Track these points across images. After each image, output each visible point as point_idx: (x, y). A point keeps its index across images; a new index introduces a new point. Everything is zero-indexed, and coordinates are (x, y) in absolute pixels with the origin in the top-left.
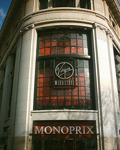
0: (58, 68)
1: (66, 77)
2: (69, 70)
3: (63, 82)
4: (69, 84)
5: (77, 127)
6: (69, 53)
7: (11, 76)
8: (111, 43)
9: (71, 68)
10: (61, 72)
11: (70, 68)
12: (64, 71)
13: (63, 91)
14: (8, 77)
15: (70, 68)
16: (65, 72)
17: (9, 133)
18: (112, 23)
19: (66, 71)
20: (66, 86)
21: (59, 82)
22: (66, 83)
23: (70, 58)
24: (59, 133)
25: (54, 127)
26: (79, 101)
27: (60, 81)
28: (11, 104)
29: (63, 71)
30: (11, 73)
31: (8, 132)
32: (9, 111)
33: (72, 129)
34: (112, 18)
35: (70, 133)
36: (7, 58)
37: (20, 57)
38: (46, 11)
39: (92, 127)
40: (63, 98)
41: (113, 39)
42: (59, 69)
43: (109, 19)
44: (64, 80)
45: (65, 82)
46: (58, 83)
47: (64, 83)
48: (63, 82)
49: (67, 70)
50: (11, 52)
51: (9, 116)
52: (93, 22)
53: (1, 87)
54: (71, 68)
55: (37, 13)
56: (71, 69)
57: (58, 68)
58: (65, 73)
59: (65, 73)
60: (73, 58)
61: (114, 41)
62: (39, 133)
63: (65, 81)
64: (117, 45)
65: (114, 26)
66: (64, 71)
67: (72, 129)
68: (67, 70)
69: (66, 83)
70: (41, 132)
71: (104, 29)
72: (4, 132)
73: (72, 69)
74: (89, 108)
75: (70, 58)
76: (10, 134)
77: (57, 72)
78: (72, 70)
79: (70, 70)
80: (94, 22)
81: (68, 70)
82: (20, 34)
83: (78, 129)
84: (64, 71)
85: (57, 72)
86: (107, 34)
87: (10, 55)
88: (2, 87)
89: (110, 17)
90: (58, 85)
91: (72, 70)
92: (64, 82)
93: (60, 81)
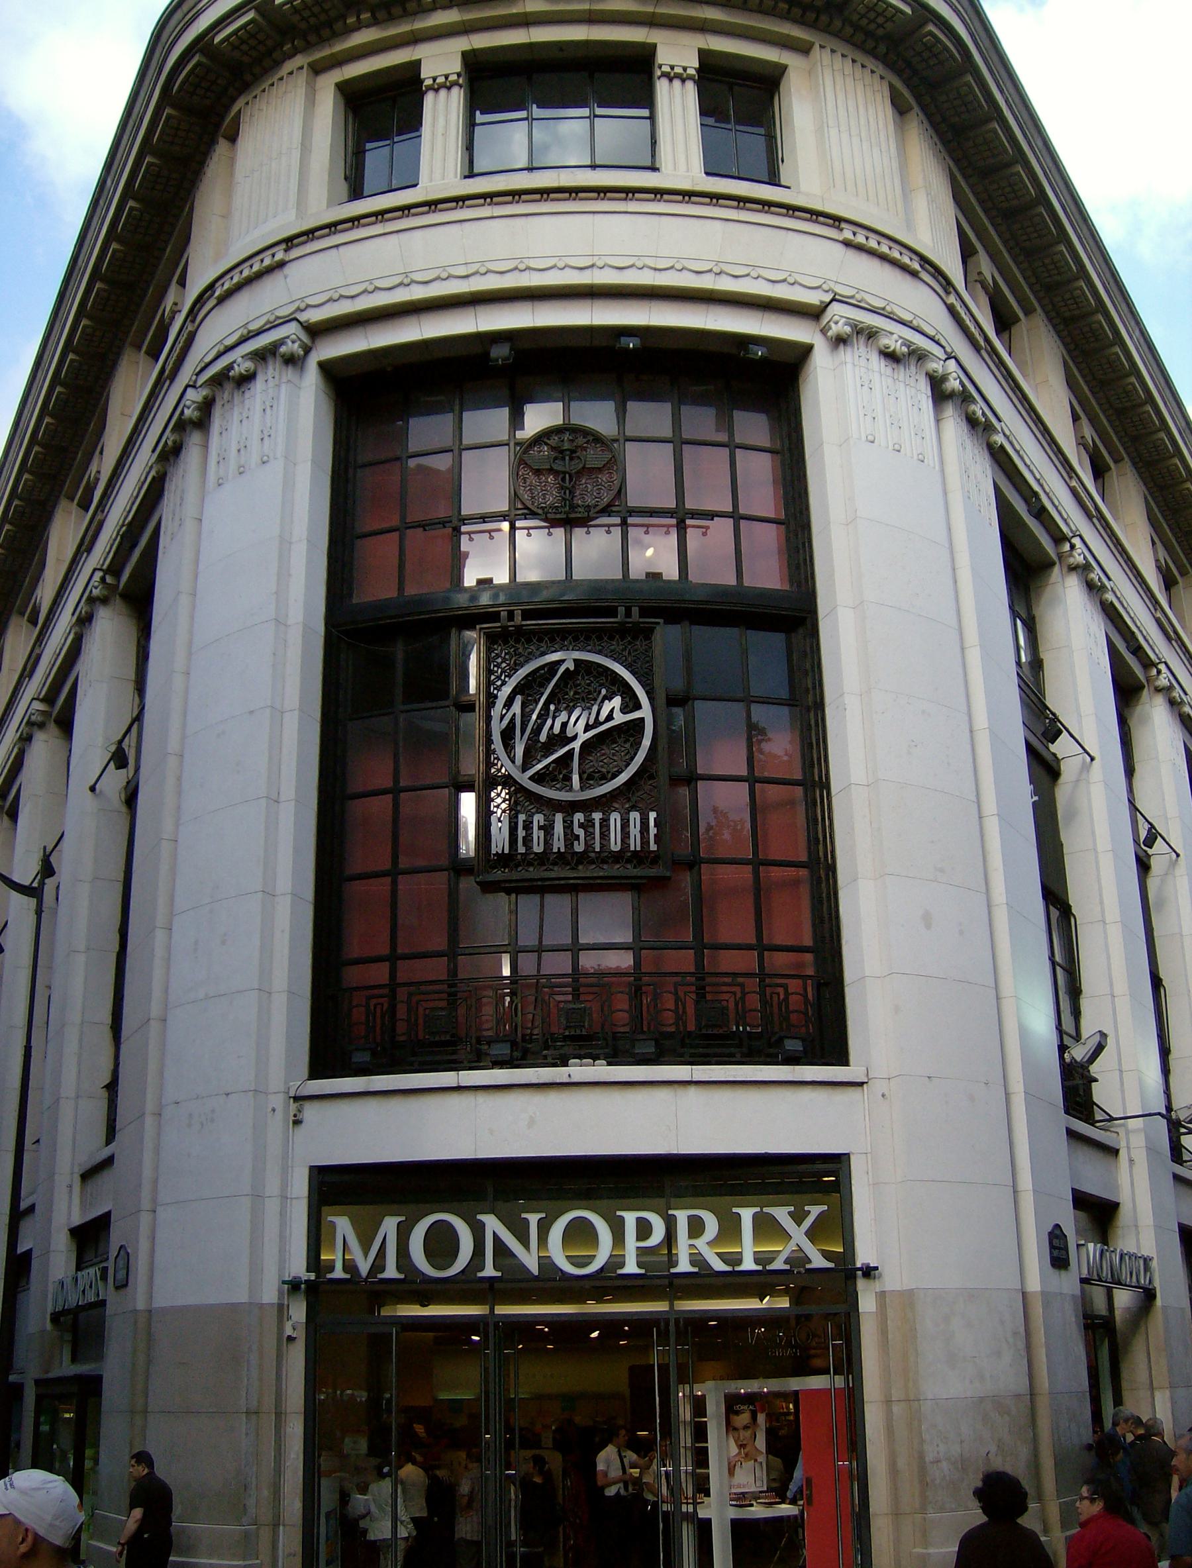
0: (517, 708)
1: (588, 779)
2: (610, 717)
3: (559, 828)
4: (538, 848)
5: (682, 1217)
6: (732, 581)
7: (115, 780)
8: (983, 474)
9: (632, 703)
10: (543, 737)
11: (617, 702)
12: (570, 734)
13: (558, 904)
14: (93, 789)
15: (617, 702)
16: (575, 737)
17: (111, 1272)
18: (984, 300)
19: (587, 728)
20: (582, 858)
21: (528, 826)
22: (589, 835)
23: (621, 610)
24: (534, 1268)
25: (492, 1223)
26: (393, 996)
27: (538, 819)
28: (120, 1037)
29: (557, 730)
30: (119, 758)
31: (105, 1271)
32: (107, 1087)
33: (644, 1229)
34: (991, 256)
35: (482, 1269)
36: (84, 621)
37: (192, 618)
38: (405, 210)
39: (815, 1211)
40: (801, 965)
41: (999, 439)
42: (525, 717)
43: (953, 268)
44: (570, 808)
45: (581, 825)
46: (521, 833)
47: (570, 837)
48: (559, 828)
49: (597, 723)
50: (114, 569)
51: (111, 1133)
52: (813, 298)
53: (42, 884)
54: (632, 703)
55: (333, 227)
56: (625, 710)
57: (517, 708)
58: (576, 745)
59: (576, 745)
60: (644, 612)
61: (1002, 458)
62: (364, 1267)
63: (579, 817)
64: (1036, 487)
65: (1004, 322)
66: (564, 725)
67: (644, 1229)
68: (597, 723)
69: (589, 835)
70: (379, 1264)
71: (919, 356)
72: (79, 1268)
73: (638, 706)
74: (793, 1045)
75: (621, 610)
76: (117, 1288)
77: (508, 735)
78: (636, 715)
79: (619, 718)
80: (827, 298)
81: (602, 717)
82: (187, 412)
83: (696, 1228)
84: (564, 725)
85: (508, 735)
86: (940, 394)
87: (104, 601)
88: (50, 883)
89: (967, 253)
90: (521, 849)
91: (636, 715)
92: (568, 826)
93: (538, 819)
